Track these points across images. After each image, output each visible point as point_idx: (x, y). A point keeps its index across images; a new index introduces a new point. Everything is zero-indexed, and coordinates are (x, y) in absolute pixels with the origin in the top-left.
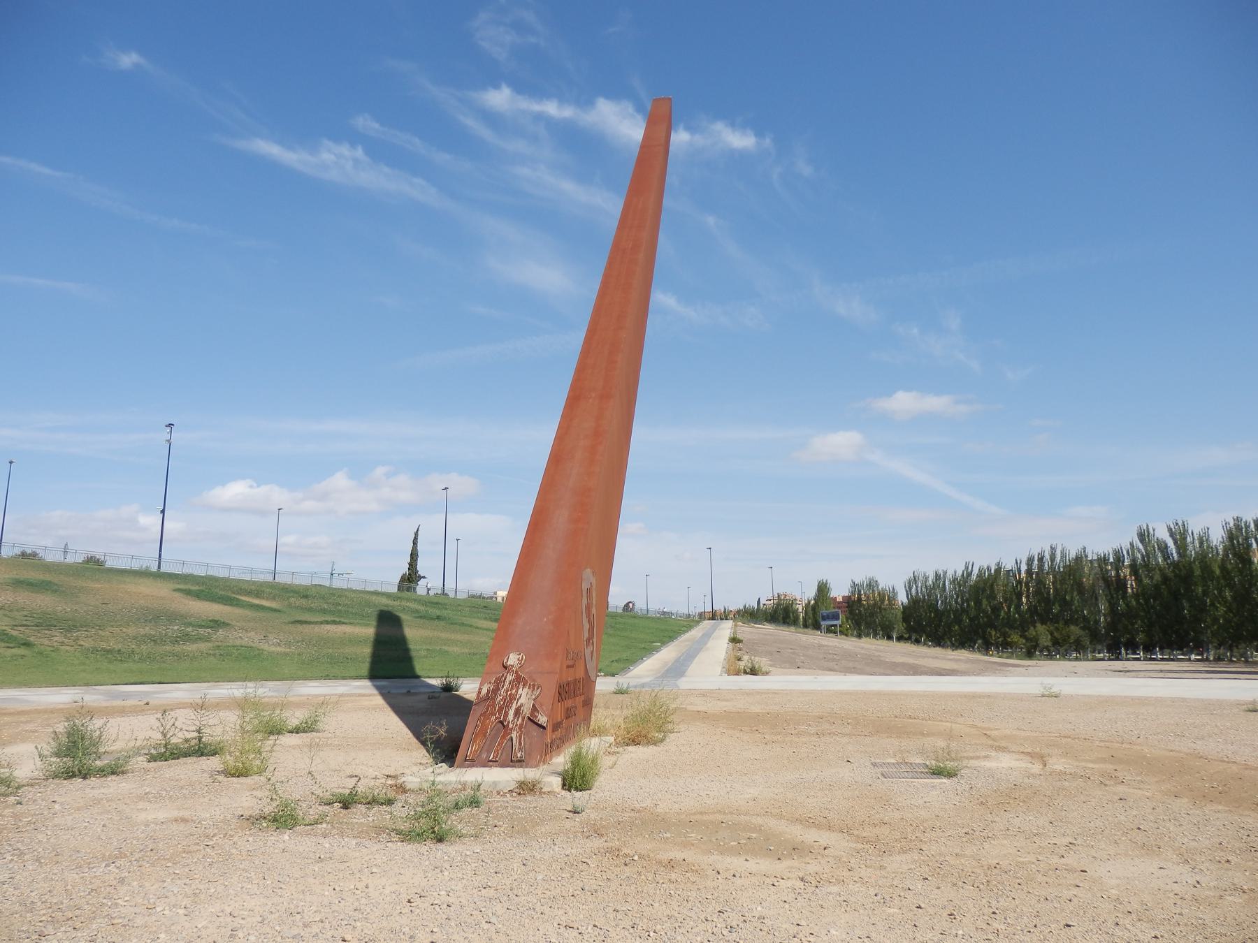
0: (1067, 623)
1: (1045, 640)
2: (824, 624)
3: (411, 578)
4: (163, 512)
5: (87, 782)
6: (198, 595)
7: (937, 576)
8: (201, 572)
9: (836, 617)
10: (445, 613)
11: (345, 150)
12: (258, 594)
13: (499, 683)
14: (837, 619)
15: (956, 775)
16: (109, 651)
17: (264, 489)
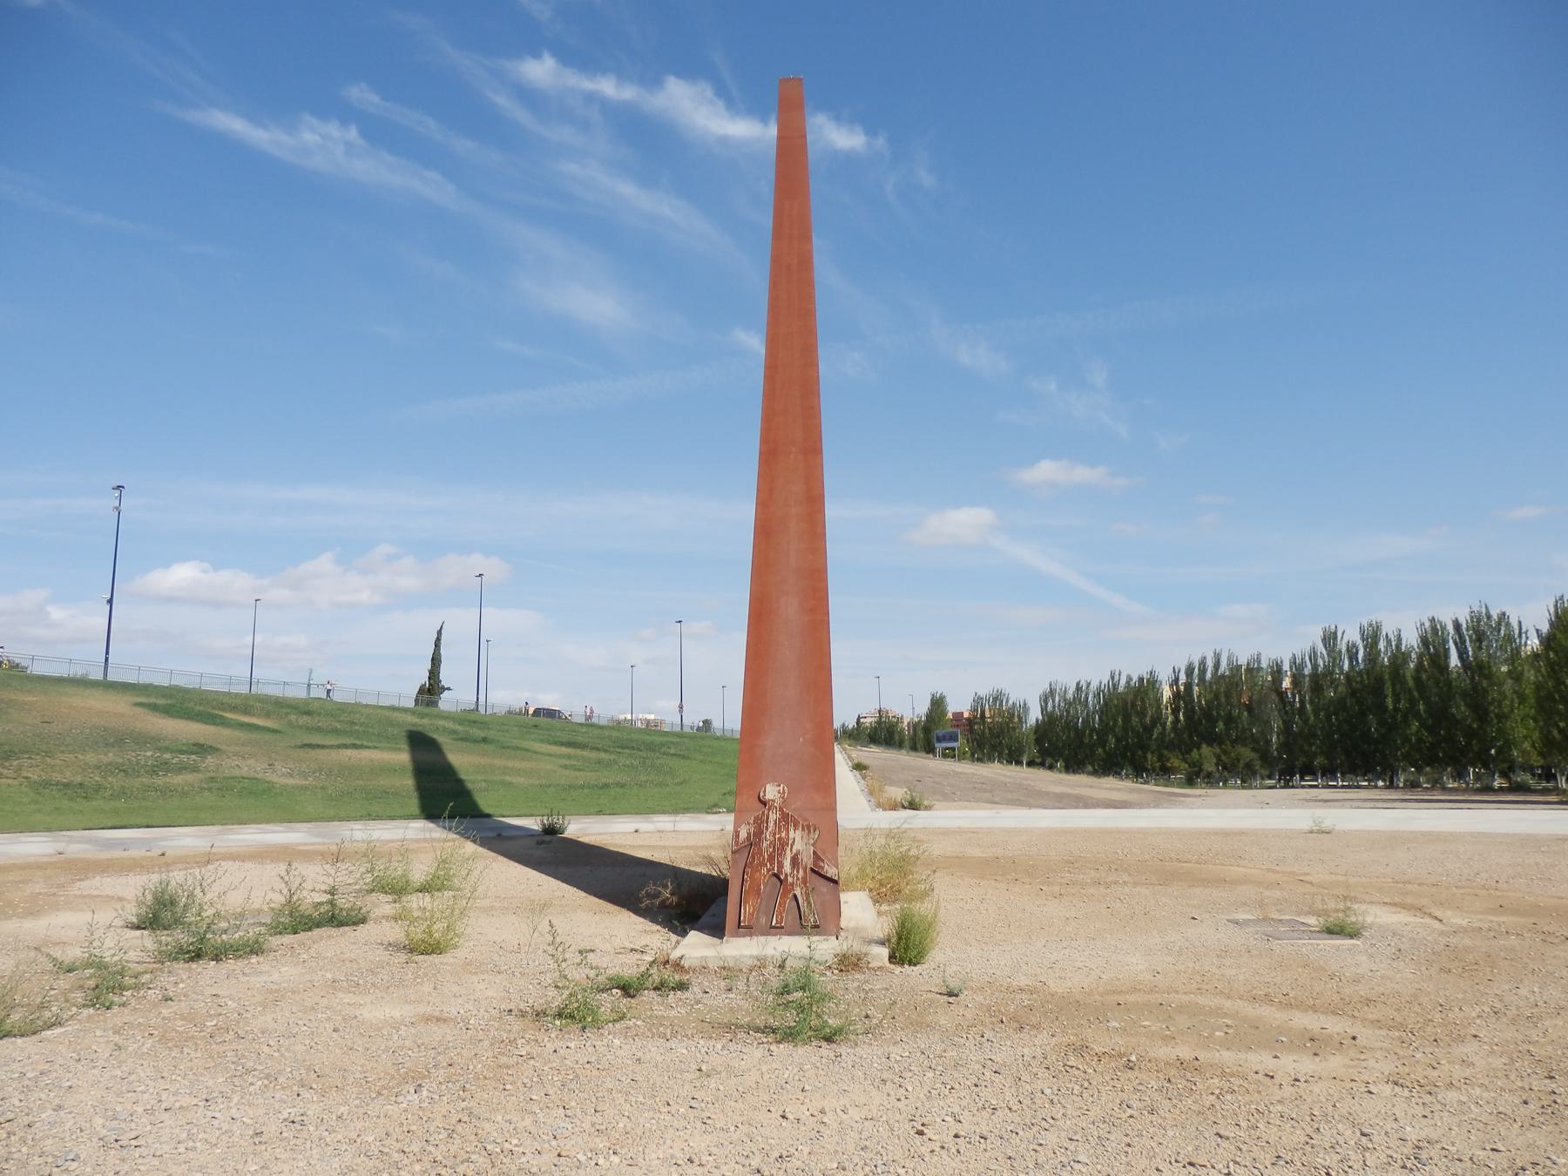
0: (1234, 742)
1: (1209, 766)
2: (939, 746)
3: (431, 690)
4: (110, 602)
5: (222, 965)
6: (167, 711)
7: (1079, 688)
8: (164, 681)
9: (953, 738)
10: (491, 734)
11: (333, 129)
12: (246, 711)
13: (760, 823)
14: (956, 740)
15: (363, 921)
16: (67, 786)
17: (225, 576)
